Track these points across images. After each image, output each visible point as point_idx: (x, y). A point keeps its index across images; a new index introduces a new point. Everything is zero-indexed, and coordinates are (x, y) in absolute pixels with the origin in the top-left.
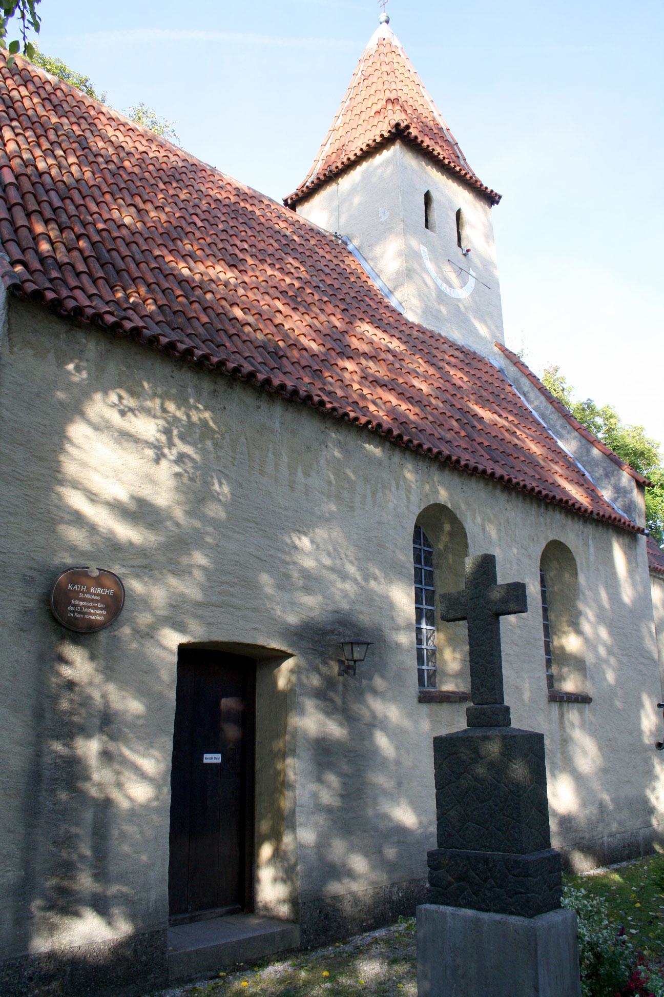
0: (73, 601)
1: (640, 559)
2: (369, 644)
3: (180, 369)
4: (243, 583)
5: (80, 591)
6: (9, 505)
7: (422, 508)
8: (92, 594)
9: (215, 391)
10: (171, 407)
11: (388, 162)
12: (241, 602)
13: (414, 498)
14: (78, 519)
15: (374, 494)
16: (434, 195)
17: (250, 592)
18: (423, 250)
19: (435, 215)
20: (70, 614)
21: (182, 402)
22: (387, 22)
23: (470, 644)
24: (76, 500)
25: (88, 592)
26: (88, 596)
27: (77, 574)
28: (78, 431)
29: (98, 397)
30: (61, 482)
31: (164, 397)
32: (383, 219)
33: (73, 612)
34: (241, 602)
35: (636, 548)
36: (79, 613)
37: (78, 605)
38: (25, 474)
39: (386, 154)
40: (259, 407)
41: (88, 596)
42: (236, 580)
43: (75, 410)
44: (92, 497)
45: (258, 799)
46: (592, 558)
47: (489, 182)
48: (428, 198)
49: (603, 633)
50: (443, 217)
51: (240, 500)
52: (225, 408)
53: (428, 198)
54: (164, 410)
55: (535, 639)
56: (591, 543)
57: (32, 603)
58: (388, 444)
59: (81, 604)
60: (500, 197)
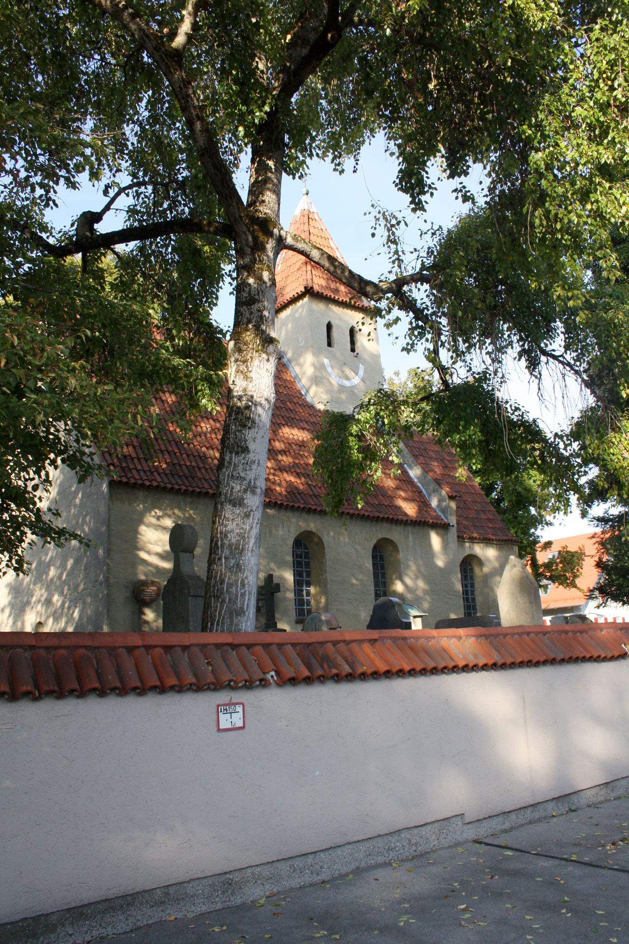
1: (450, 540)
10: (176, 511)
11: (302, 306)
13: (293, 530)
14: (145, 562)
15: (270, 531)
16: (333, 323)
18: (326, 361)
19: (335, 333)
21: (180, 509)
22: (307, 194)
23: (169, 581)
24: (143, 555)
27: (144, 583)
28: (143, 529)
29: (148, 515)
30: (139, 549)
31: (172, 509)
32: (302, 344)
39: (300, 303)
43: (141, 522)
44: (149, 553)
46: (411, 544)
48: (329, 327)
49: (421, 584)
50: (341, 337)
53: (329, 327)
54: (174, 513)
56: (410, 535)
57: (128, 594)
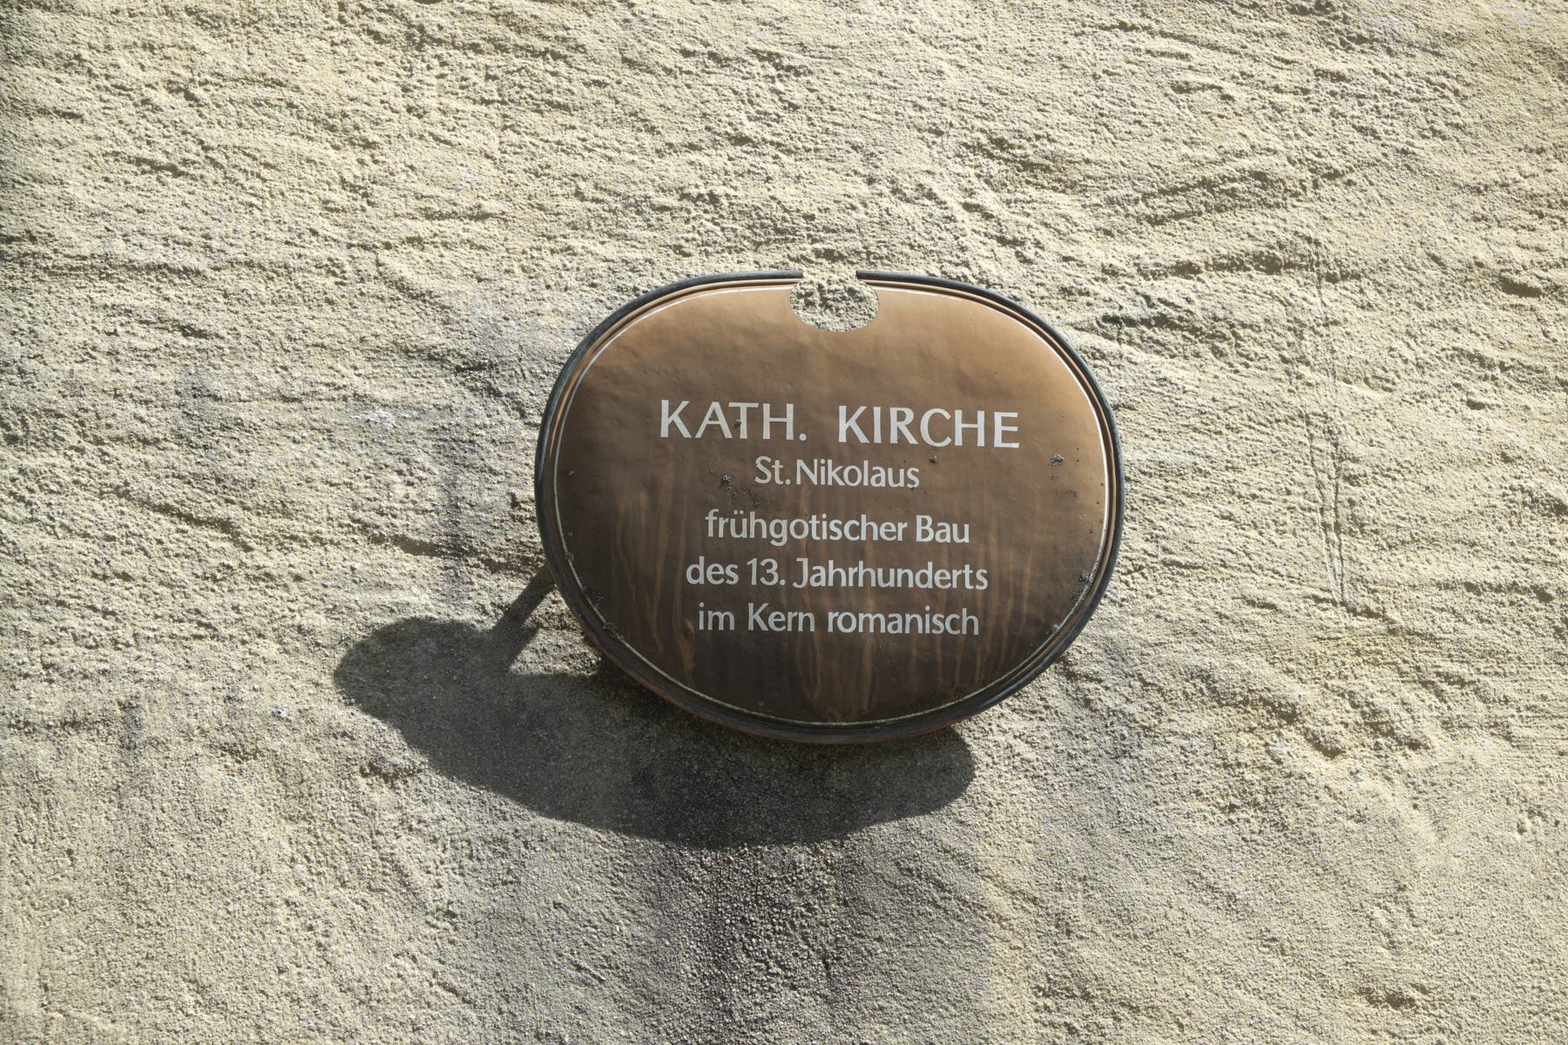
5: (756, 446)
8: (851, 453)
25: (820, 445)
26: (829, 474)
36: (776, 599)
37: (760, 547)
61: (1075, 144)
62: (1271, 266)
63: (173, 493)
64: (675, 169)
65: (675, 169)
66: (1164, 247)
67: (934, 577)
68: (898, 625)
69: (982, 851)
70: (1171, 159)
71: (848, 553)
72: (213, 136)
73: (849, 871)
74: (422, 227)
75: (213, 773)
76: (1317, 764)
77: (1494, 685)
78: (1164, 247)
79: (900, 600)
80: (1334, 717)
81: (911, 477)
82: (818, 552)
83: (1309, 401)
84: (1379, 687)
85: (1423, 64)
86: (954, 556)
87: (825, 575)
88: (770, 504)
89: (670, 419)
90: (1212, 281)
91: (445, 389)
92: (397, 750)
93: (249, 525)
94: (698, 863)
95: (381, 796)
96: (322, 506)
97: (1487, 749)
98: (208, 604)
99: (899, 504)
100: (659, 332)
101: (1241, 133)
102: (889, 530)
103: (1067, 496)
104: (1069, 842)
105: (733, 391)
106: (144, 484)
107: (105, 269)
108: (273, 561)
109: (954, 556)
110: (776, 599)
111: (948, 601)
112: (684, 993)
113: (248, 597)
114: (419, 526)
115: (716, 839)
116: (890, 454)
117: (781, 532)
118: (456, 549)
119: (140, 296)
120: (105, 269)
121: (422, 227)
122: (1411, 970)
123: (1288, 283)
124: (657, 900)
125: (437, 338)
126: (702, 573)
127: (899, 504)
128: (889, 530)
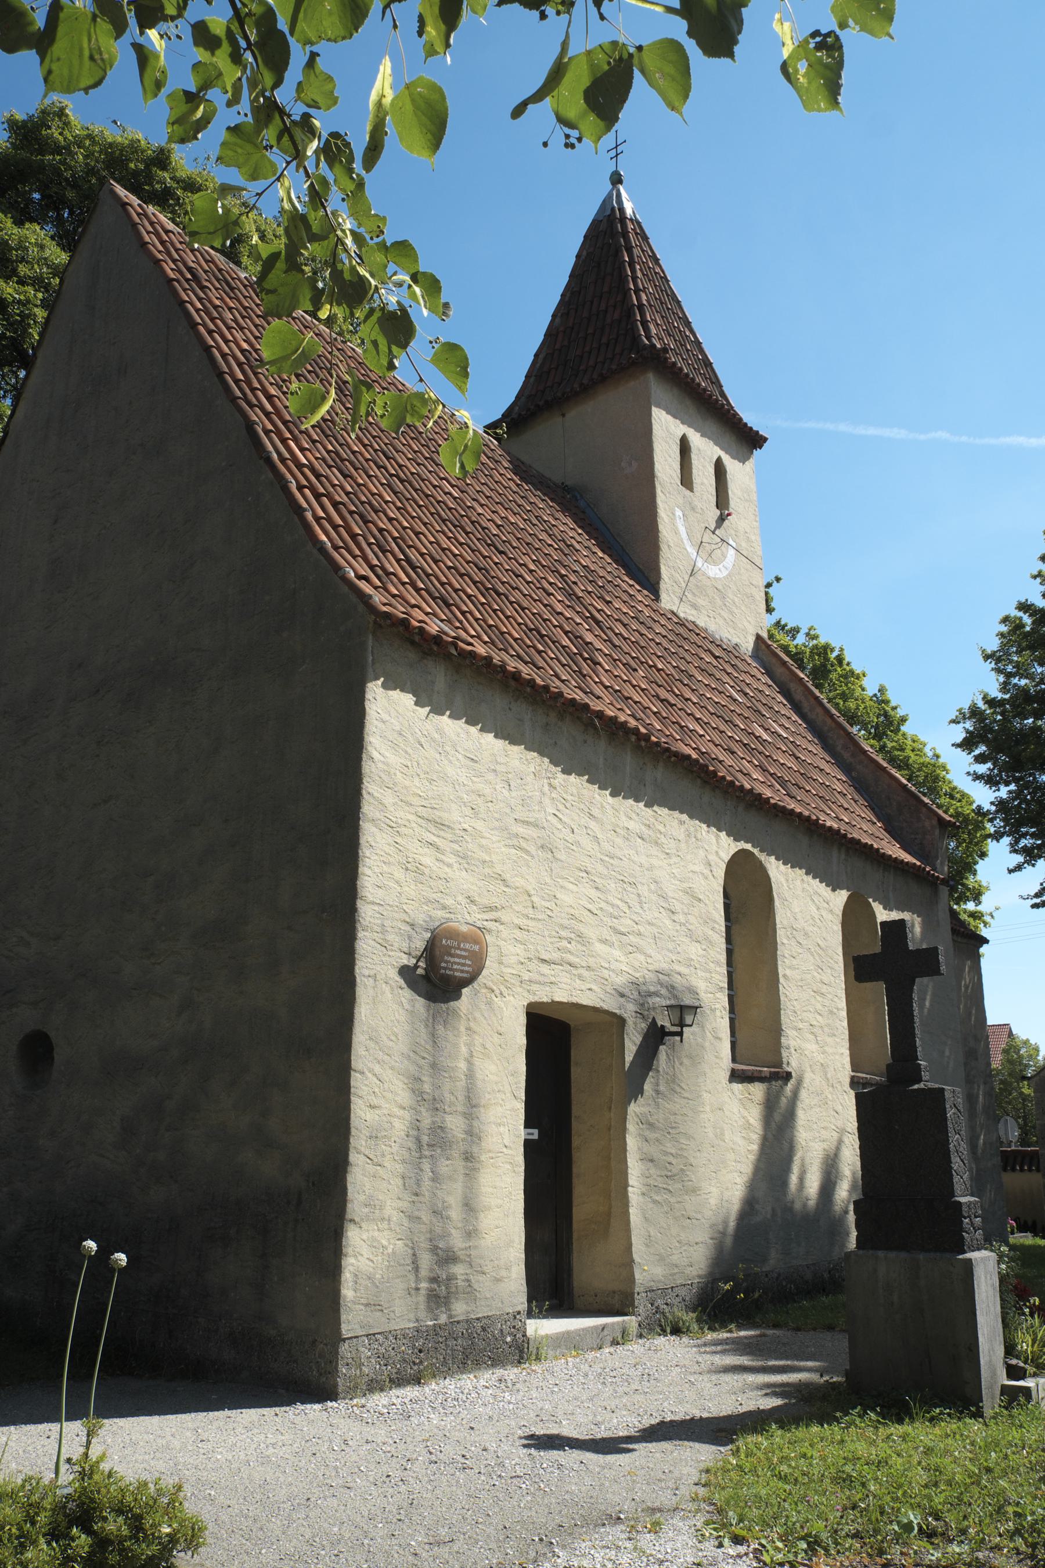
0: (446, 958)
2: (697, 1008)
3: (516, 701)
4: (578, 939)
5: (452, 947)
6: (383, 854)
7: (731, 855)
8: (461, 950)
9: (547, 724)
12: (577, 960)
17: (584, 949)
20: (442, 971)
25: (459, 948)
26: (458, 952)
33: (445, 969)
34: (577, 960)
35: (937, 903)
36: (451, 970)
37: (449, 962)
38: (394, 819)
40: (585, 742)
41: (458, 952)
42: (573, 936)
45: (575, 1181)
47: (750, 418)
51: (572, 847)
52: (556, 743)
55: (838, 1009)
58: (699, 781)
59: (452, 960)
60: (765, 439)
61: (477, 899)
62: (496, 921)
63: (380, 941)
64: (434, 895)
65: (434, 895)
66: (486, 916)
67: (466, 968)
68: (461, 975)
69: (462, 1008)
70: (487, 902)
71: (458, 964)
72: (385, 882)
73: (448, 1009)
74: (407, 901)
75: (384, 985)
76: (494, 998)
77: (514, 989)
78: (486, 916)
79: (462, 971)
80: (497, 992)
81: (466, 954)
82: (456, 963)
83: (498, 943)
84: (502, 988)
85: (514, 891)
86: (469, 966)
87: (455, 967)
88: (452, 956)
89: (444, 942)
90: (489, 922)
91: (408, 928)
92: (404, 985)
93: (388, 947)
94: (432, 1005)
95: (400, 991)
96: (396, 945)
97: (512, 998)
98: (384, 959)
99: (464, 958)
100: (444, 928)
101: (495, 899)
102: (463, 961)
103: (482, 958)
104: (470, 1007)
105: (451, 939)
106: (377, 939)
107: (373, 903)
108: (390, 953)
109: (469, 966)
110: (451, 970)
111: (467, 972)
112: (430, 1025)
113: (387, 958)
114: (406, 950)
115: (434, 1002)
116: (465, 950)
117: (452, 960)
118: (410, 954)
119: (376, 908)
120: (373, 903)
121: (407, 901)
122: (502, 1030)
123: (497, 924)
124: (428, 1010)
125: (408, 920)
126: (443, 965)
127: (464, 958)
128: (463, 961)
